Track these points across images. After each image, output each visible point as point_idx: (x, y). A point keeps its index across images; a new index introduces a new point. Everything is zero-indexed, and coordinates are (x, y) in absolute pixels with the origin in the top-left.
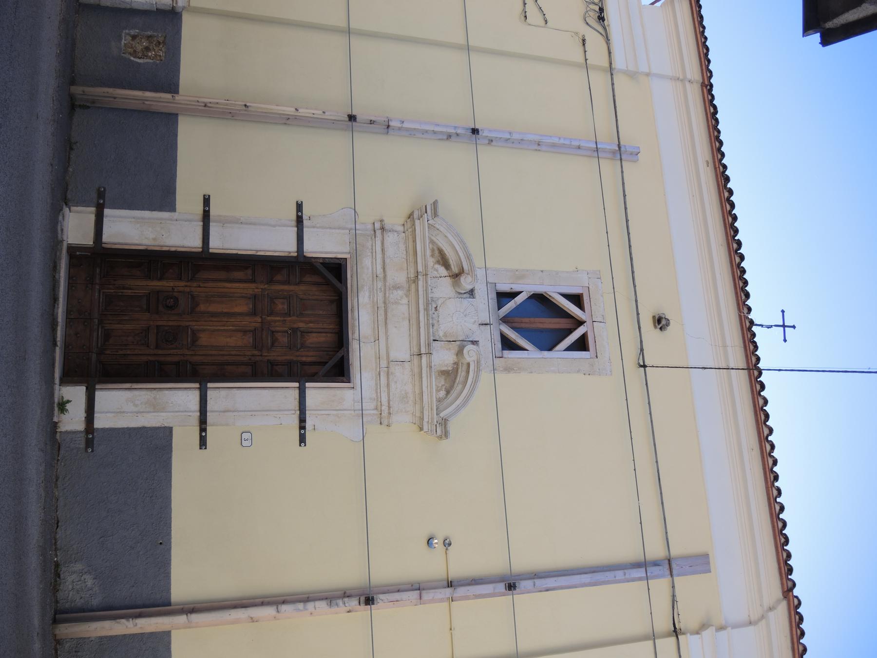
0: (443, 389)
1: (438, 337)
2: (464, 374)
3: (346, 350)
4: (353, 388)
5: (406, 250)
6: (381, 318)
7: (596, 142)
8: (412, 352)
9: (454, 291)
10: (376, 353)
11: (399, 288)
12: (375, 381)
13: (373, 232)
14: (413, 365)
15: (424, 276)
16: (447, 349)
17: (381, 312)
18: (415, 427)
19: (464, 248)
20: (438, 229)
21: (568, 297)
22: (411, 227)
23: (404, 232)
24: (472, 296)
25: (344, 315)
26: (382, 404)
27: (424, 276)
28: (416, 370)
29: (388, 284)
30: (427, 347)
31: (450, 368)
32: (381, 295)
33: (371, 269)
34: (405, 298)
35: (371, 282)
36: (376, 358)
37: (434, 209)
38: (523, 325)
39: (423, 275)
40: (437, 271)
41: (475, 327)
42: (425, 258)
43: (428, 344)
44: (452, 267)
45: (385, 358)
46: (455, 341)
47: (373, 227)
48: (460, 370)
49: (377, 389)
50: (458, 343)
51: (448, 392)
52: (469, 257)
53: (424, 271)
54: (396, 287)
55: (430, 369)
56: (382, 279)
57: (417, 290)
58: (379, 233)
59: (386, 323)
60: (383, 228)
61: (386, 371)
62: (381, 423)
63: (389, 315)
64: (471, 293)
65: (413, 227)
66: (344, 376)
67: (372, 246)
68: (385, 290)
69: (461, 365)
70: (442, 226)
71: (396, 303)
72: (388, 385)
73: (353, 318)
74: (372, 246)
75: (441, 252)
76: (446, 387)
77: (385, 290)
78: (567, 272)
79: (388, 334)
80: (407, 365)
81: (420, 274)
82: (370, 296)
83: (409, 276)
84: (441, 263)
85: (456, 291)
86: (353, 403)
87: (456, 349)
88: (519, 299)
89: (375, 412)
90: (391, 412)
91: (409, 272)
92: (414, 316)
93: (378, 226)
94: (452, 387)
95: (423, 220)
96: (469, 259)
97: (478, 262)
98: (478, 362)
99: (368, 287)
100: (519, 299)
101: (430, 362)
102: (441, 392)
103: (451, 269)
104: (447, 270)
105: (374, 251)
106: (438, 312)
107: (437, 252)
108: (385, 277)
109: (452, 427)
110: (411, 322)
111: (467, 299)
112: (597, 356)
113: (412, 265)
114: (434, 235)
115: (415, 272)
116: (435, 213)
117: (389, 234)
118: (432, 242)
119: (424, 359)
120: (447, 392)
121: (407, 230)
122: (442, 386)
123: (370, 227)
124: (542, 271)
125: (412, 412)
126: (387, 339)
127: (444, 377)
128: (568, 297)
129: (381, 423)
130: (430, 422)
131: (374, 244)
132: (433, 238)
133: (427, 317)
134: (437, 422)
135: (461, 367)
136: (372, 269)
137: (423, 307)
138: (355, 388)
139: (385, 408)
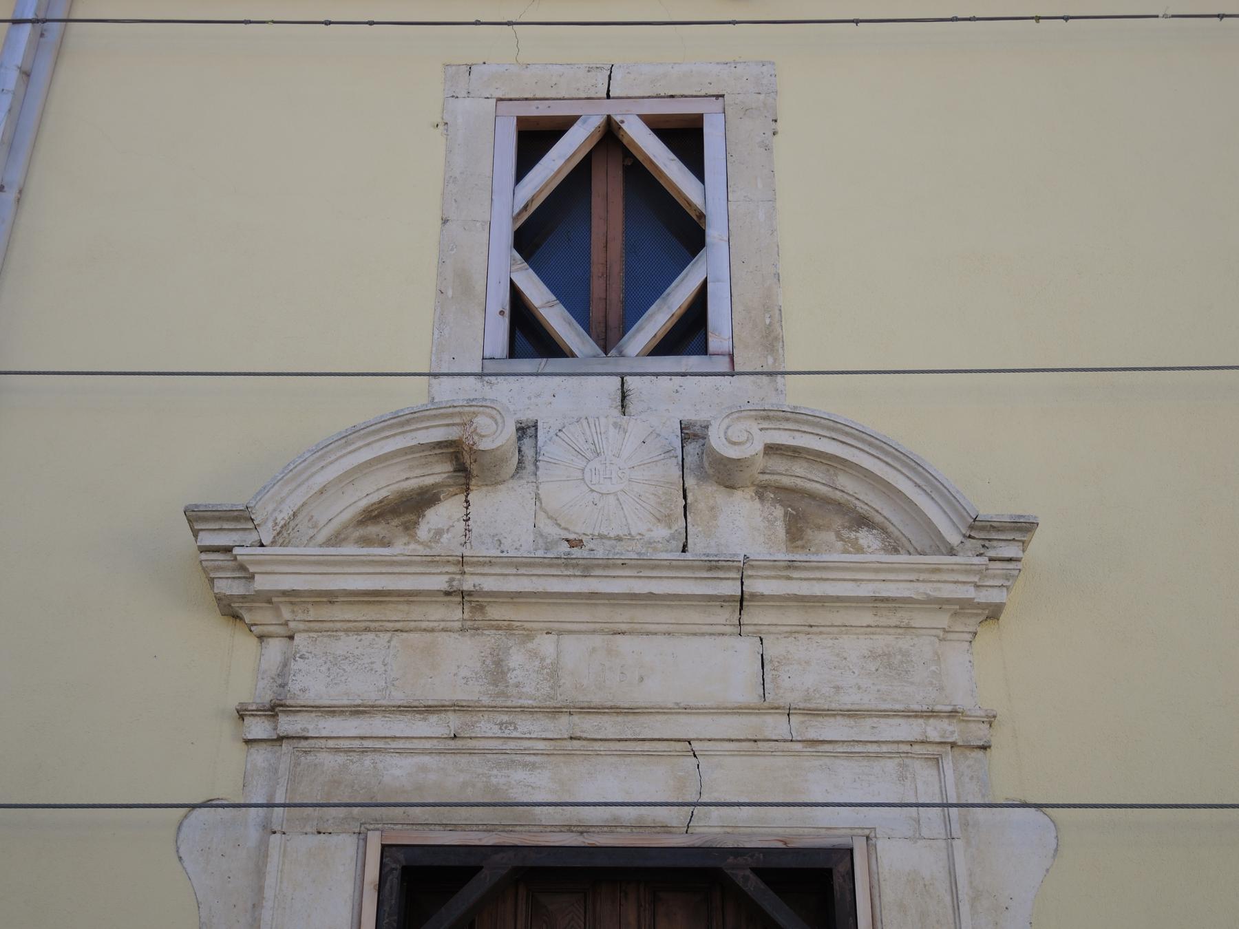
0: (853, 535)
1: (674, 543)
2: (799, 468)
3: (731, 860)
4: (868, 838)
5: (358, 631)
6: (609, 726)
7: (16, 22)
8: (728, 629)
9: (511, 483)
10: (739, 753)
11: (498, 663)
12: (838, 762)
13: (286, 746)
14: (772, 629)
15: (467, 569)
16: (715, 517)
17: (588, 725)
18: (987, 635)
19: (369, 434)
20: (295, 515)
21: (525, 163)
22: (277, 609)
23: (291, 638)
24: (531, 431)
25: (600, 862)
26: (920, 738)
27: (467, 569)
28: (794, 617)
29: (486, 701)
30: (721, 574)
31: (779, 512)
32: (527, 725)
33: (426, 759)
34: (536, 641)
35: (476, 758)
36: (753, 754)
37: (220, 519)
38: (616, 296)
39: (463, 573)
40: (439, 533)
41: (636, 427)
42: (401, 564)
43: (710, 569)
44: (429, 481)
45: (754, 720)
46: (684, 491)
47: (264, 745)
48: (786, 481)
49: (867, 756)
50: (690, 482)
51: (863, 521)
52: (403, 421)
53: (446, 569)
54: (497, 671)
55: (796, 568)
56: (467, 718)
57: (515, 598)
58: (287, 724)
59: (632, 711)
60: (272, 708)
61: (801, 718)
62: (984, 748)
63: (596, 699)
64: (526, 430)
65: (275, 599)
66: (829, 872)
67: (337, 750)
68: (509, 710)
69: (767, 477)
70: (283, 500)
71: (554, 673)
72: (852, 714)
73: (611, 828)
74: (337, 750)
75: (373, 515)
76: (844, 527)
77: (509, 710)
78: (449, 151)
79: (671, 705)
80: (774, 649)
81: (455, 583)
82: (525, 765)
83: (457, 625)
84: (414, 518)
85: (513, 477)
86: (920, 843)
87: (711, 488)
88: (537, 293)
89: (948, 764)
90: (949, 708)
91: (443, 625)
92: (602, 614)
93: (258, 728)
94: (841, 508)
95: (259, 563)
96: (408, 422)
97: (413, 394)
98: (767, 416)
99: (495, 772)
100: (537, 293)
101: (774, 568)
102: (861, 541)
103: (434, 486)
104: (439, 500)
105: (356, 744)
106: (584, 539)
107: (373, 530)
108: (459, 708)
109: (990, 509)
110: (624, 627)
111: (540, 444)
112: (718, 97)
113: (416, 612)
114: (311, 533)
115: (443, 603)
116: (237, 519)
117: (294, 687)
118: (336, 539)
119: (756, 586)
120: (859, 526)
121: (286, 624)
122: (839, 536)
123: (260, 756)
124: (445, 221)
125: (937, 640)
126: (688, 710)
127: (809, 531)
128: (525, 163)
129: (984, 748)
130: (976, 579)
131: (331, 743)
132: (323, 536)
133: (615, 566)
134: (980, 555)
135: (775, 477)
136: (424, 752)
137: (578, 580)
138: (867, 832)
139: (934, 730)
